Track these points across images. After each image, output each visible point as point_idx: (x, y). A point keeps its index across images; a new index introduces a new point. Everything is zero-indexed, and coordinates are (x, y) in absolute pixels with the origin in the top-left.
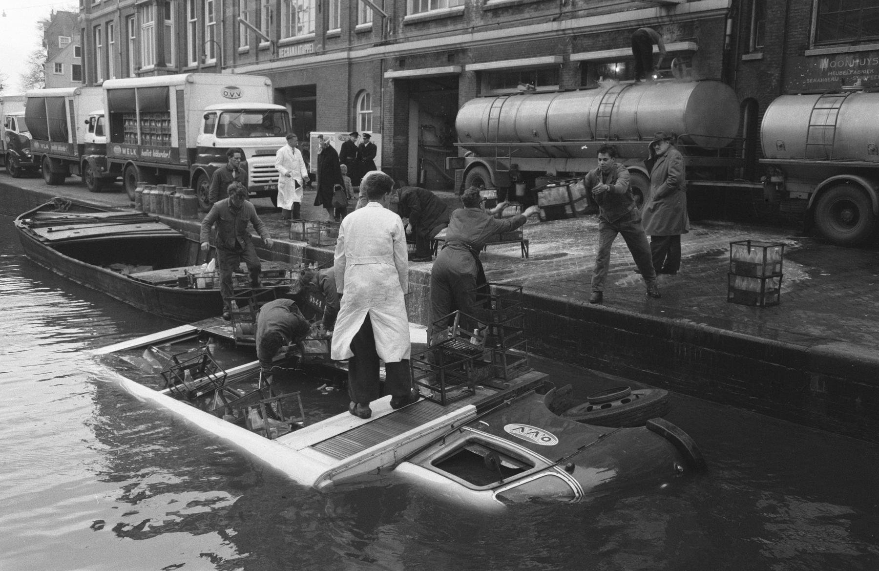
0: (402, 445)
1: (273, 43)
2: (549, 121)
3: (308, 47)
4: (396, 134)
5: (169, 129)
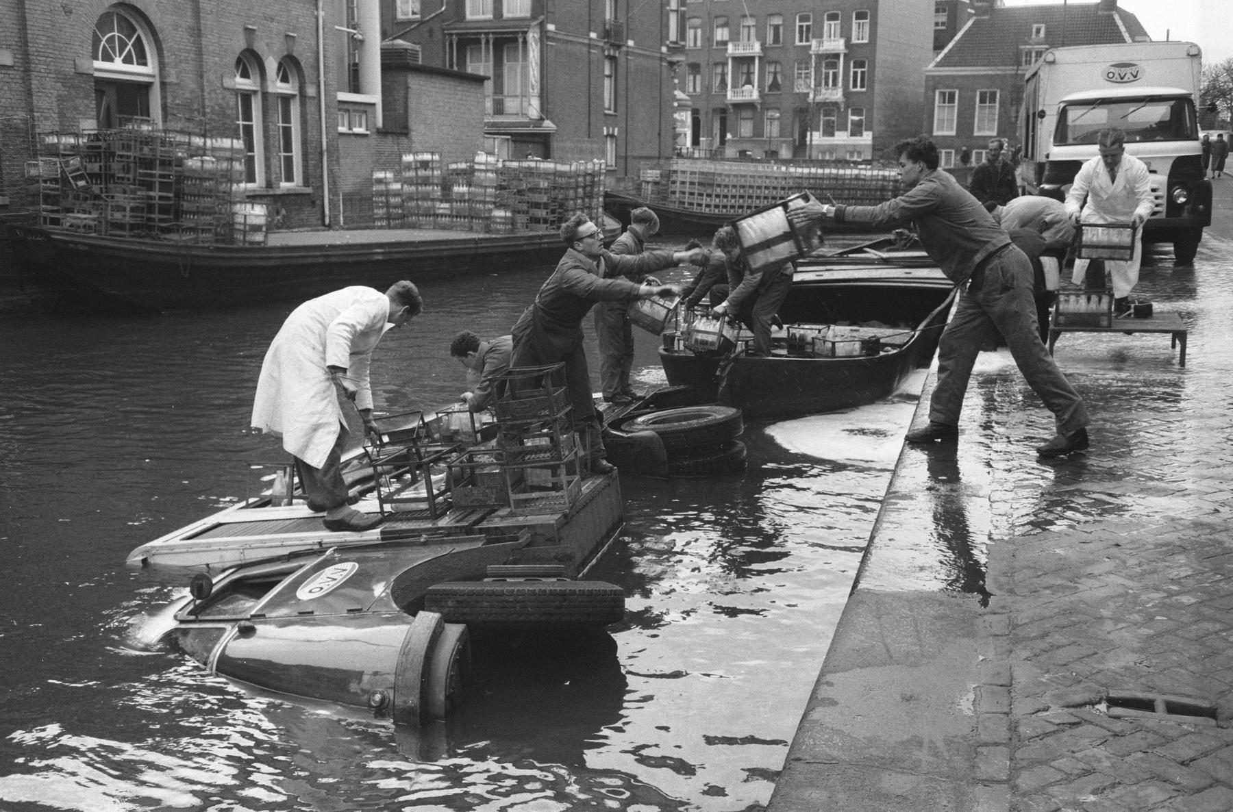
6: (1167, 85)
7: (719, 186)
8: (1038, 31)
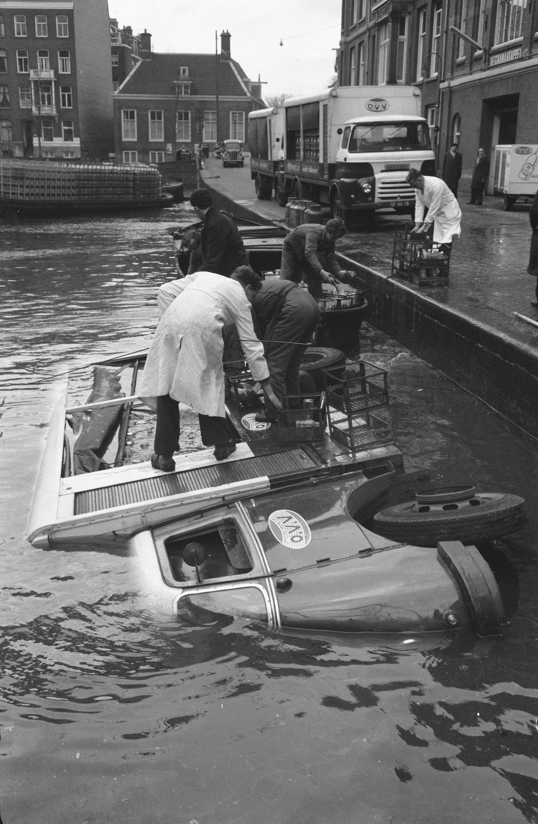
0: (152, 511)
1: (485, 50)
3: (516, 53)
5: (317, 145)
6: (404, 113)
7: (28, 179)
8: (184, 71)
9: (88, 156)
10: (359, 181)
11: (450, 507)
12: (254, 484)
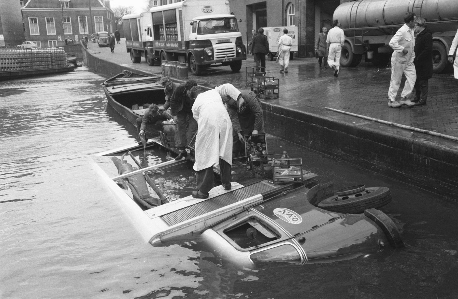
0: (209, 218)
2: (386, 13)
4: (307, 26)
5: (177, 32)
9: (9, 45)
10: (206, 49)
11: (358, 195)
12: (256, 199)
